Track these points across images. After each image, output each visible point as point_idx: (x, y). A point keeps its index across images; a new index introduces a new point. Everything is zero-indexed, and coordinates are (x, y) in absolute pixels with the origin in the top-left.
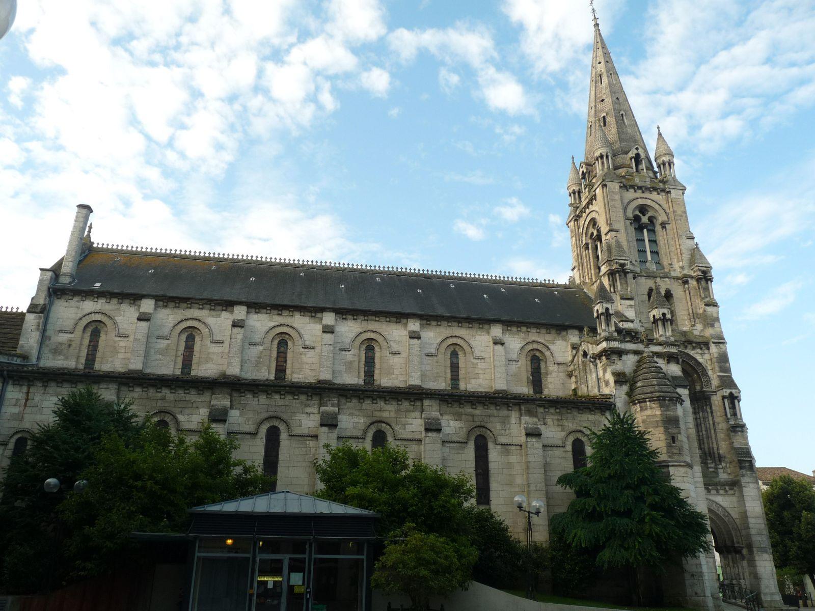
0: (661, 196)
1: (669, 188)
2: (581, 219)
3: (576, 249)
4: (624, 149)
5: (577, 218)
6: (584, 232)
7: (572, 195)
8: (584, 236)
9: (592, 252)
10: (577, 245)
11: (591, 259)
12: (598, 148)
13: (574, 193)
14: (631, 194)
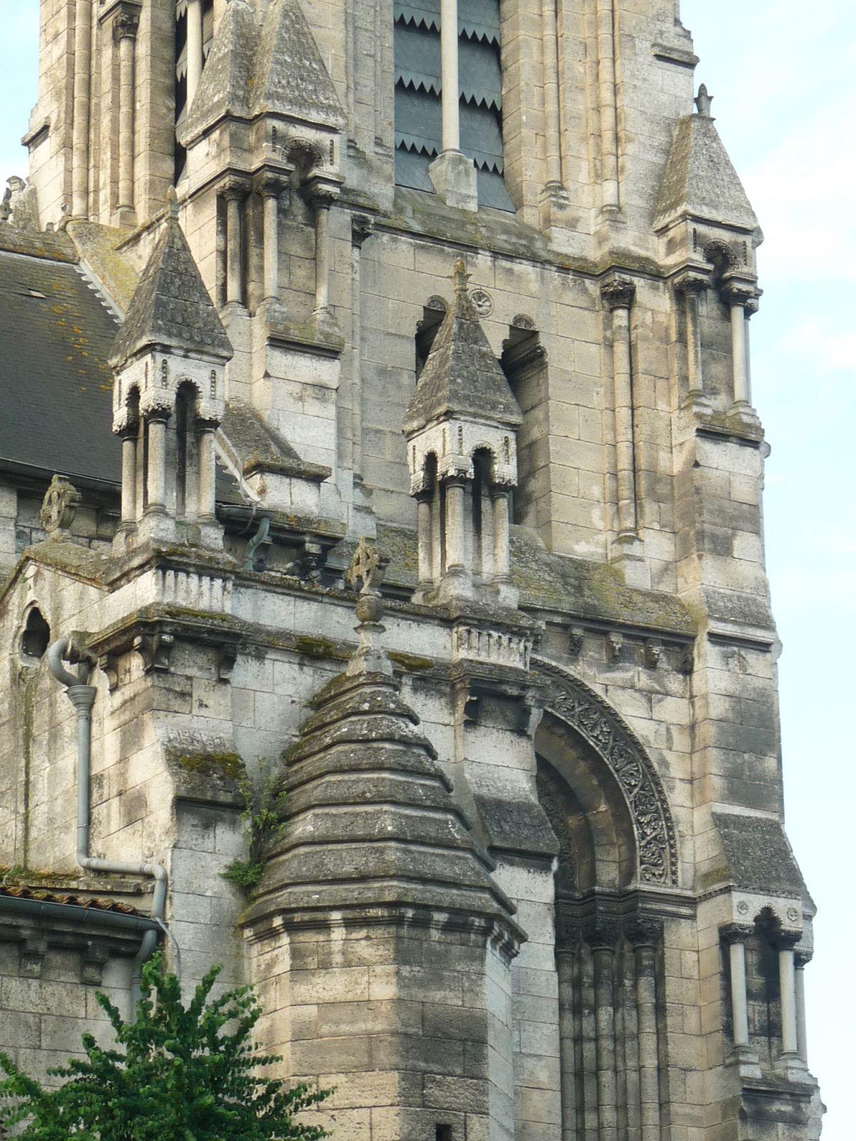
3: (62, 25)
11: (144, 94)
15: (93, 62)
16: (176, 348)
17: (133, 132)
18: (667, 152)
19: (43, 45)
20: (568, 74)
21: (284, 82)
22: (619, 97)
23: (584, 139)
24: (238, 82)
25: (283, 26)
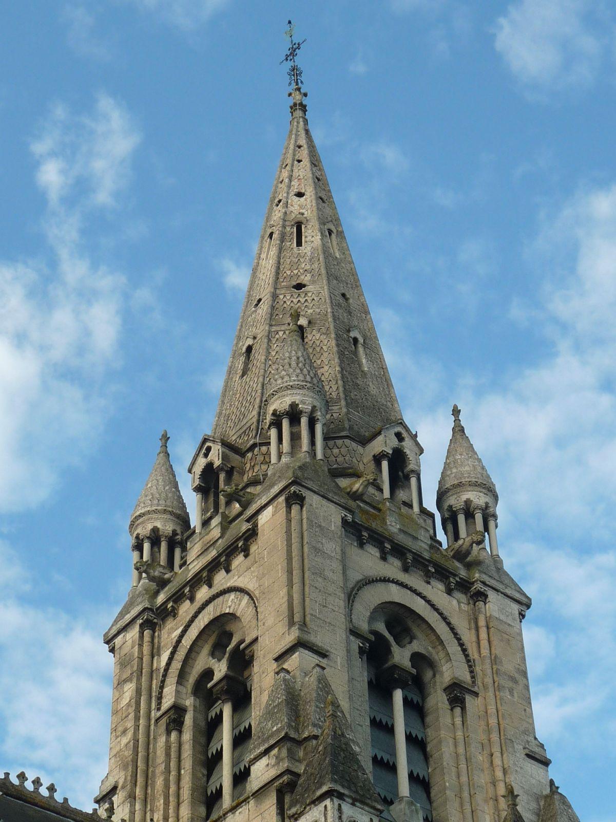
0: (455, 602)
1: (484, 583)
2: (170, 623)
3: (130, 724)
4: (356, 428)
5: (153, 619)
6: (176, 665)
7: (146, 546)
8: (172, 680)
9: (195, 740)
10: (137, 710)
11: (187, 764)
12: (287, 388)
13: (155, 538)
14: (369, 561)
15: (151, 746)
16: (347, 796)
17: (179, 788)
18: (538, 815)
19: (113, 738)
20: (473, 760)
21: (322, 719)
22: (507, 776)
23: (486, 801)
24: (291, 718)
25: (318, 688)
